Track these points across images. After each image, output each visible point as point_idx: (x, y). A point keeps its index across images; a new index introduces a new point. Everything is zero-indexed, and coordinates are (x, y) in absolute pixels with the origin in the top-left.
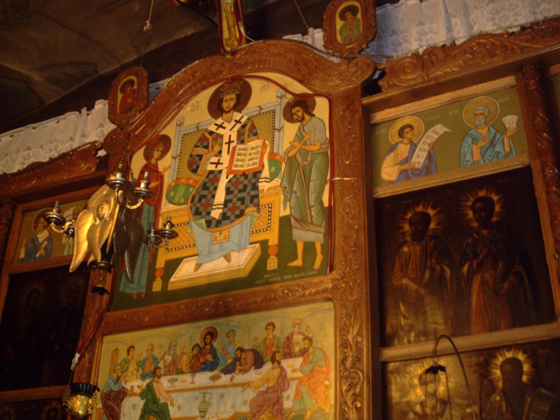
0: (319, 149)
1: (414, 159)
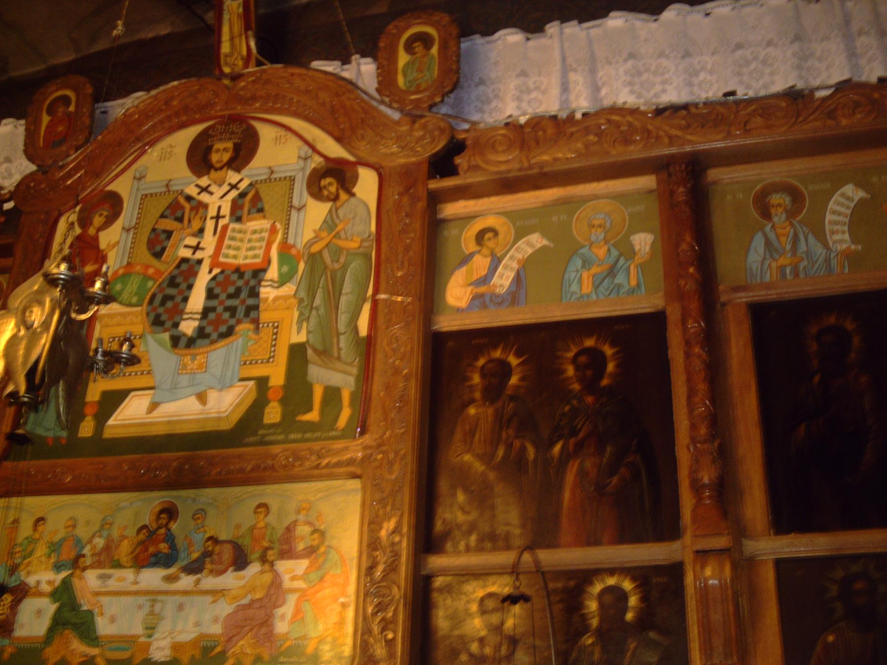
0: (359, 248)
1: (495, 280)
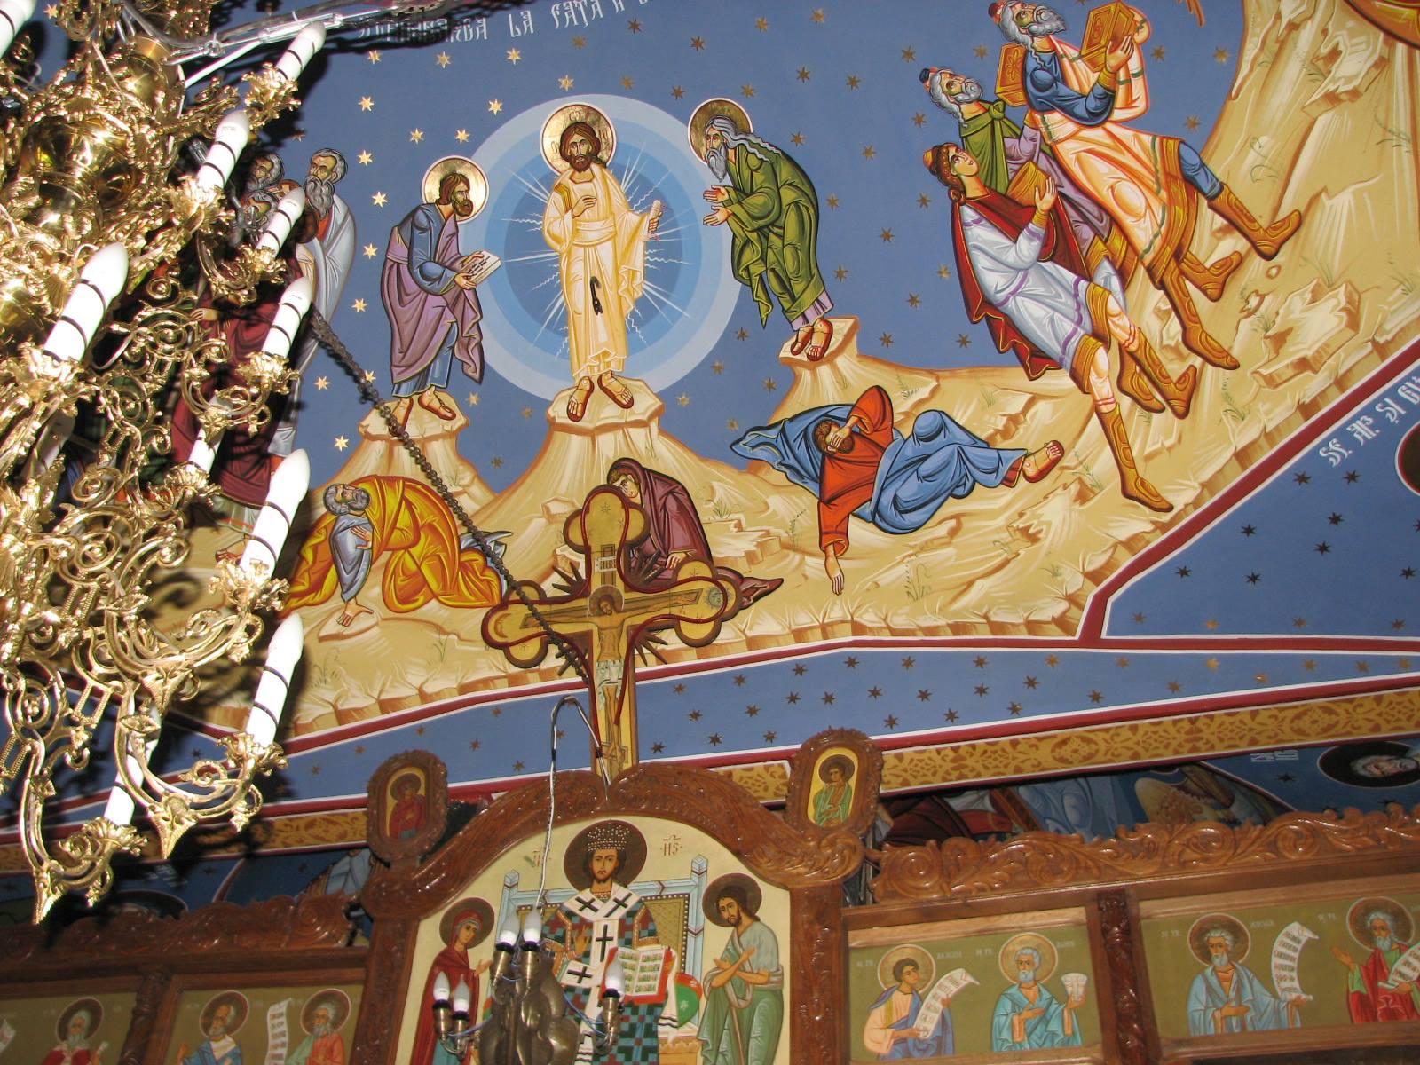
1: (919, 1023)
